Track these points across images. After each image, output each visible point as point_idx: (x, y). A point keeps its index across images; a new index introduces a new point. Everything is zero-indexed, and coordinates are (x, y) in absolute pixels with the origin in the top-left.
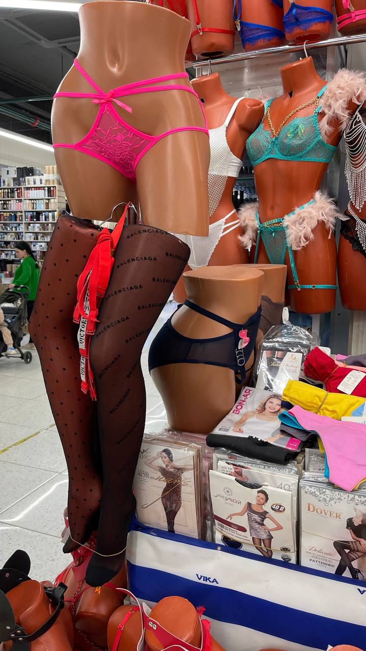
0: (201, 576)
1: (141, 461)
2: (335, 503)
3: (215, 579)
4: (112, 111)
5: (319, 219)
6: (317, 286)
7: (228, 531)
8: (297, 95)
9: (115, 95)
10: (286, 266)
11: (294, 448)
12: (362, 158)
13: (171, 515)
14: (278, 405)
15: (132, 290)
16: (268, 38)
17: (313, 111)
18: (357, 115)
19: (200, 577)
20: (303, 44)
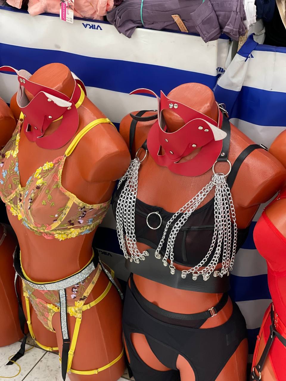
0: (97, 29)
3: (86, 27)
19: (99, 28)
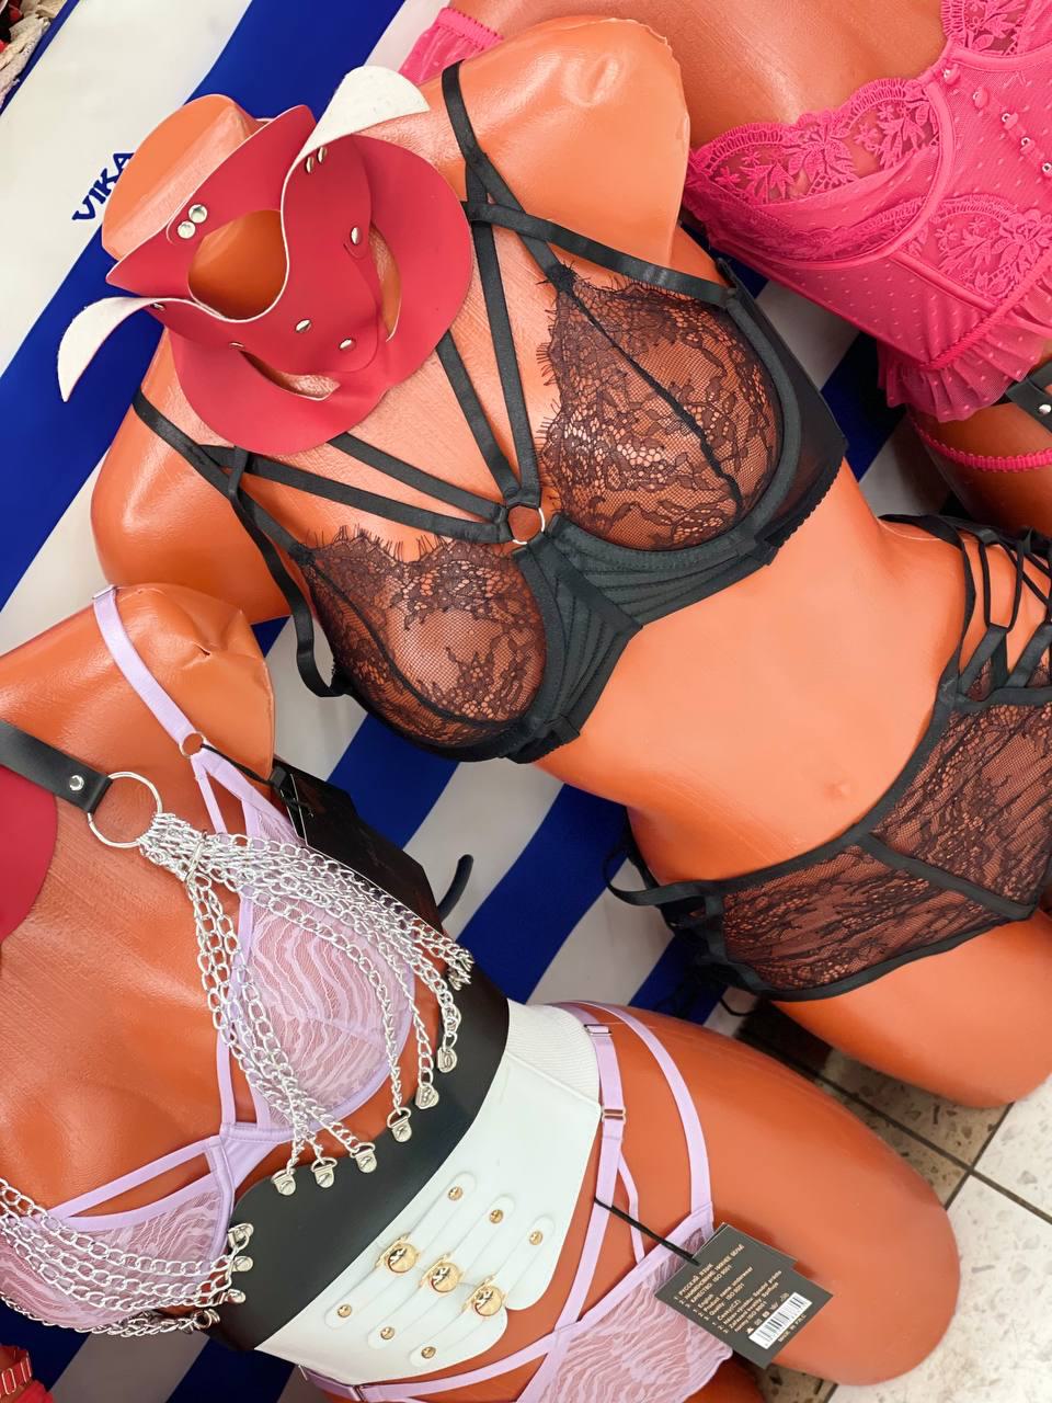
0: (87, 202)
3: (116, 157)
19: (85, 210)
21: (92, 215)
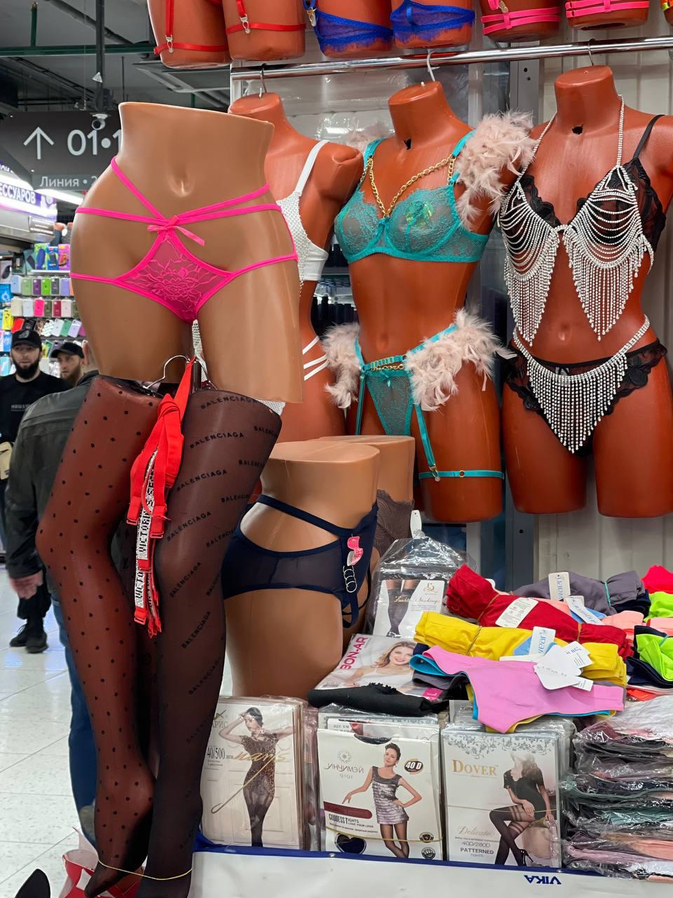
0: (552, 883)
1: (215, 731)
2: (488, 752)
3: (530, 882)
4: (177, 243)
5: (465, 358)
6: (468, 473)
7: (345, 825)
8: (418, 147)
9: (177, 223)
10: (413, 439)
11: (433, 697)
12: (528, 258)
13: (258, 811)
14: (409, 655)
15: (214, 476)
16: (364, 42)
17: (444, 181)
18: (517, 188)
19: (555, 881)
20: (426, 58)
21: (555, 878)
